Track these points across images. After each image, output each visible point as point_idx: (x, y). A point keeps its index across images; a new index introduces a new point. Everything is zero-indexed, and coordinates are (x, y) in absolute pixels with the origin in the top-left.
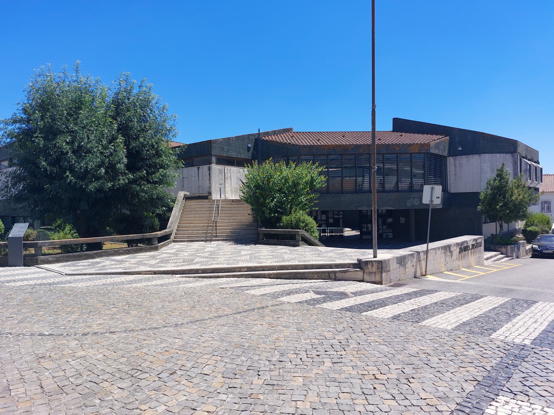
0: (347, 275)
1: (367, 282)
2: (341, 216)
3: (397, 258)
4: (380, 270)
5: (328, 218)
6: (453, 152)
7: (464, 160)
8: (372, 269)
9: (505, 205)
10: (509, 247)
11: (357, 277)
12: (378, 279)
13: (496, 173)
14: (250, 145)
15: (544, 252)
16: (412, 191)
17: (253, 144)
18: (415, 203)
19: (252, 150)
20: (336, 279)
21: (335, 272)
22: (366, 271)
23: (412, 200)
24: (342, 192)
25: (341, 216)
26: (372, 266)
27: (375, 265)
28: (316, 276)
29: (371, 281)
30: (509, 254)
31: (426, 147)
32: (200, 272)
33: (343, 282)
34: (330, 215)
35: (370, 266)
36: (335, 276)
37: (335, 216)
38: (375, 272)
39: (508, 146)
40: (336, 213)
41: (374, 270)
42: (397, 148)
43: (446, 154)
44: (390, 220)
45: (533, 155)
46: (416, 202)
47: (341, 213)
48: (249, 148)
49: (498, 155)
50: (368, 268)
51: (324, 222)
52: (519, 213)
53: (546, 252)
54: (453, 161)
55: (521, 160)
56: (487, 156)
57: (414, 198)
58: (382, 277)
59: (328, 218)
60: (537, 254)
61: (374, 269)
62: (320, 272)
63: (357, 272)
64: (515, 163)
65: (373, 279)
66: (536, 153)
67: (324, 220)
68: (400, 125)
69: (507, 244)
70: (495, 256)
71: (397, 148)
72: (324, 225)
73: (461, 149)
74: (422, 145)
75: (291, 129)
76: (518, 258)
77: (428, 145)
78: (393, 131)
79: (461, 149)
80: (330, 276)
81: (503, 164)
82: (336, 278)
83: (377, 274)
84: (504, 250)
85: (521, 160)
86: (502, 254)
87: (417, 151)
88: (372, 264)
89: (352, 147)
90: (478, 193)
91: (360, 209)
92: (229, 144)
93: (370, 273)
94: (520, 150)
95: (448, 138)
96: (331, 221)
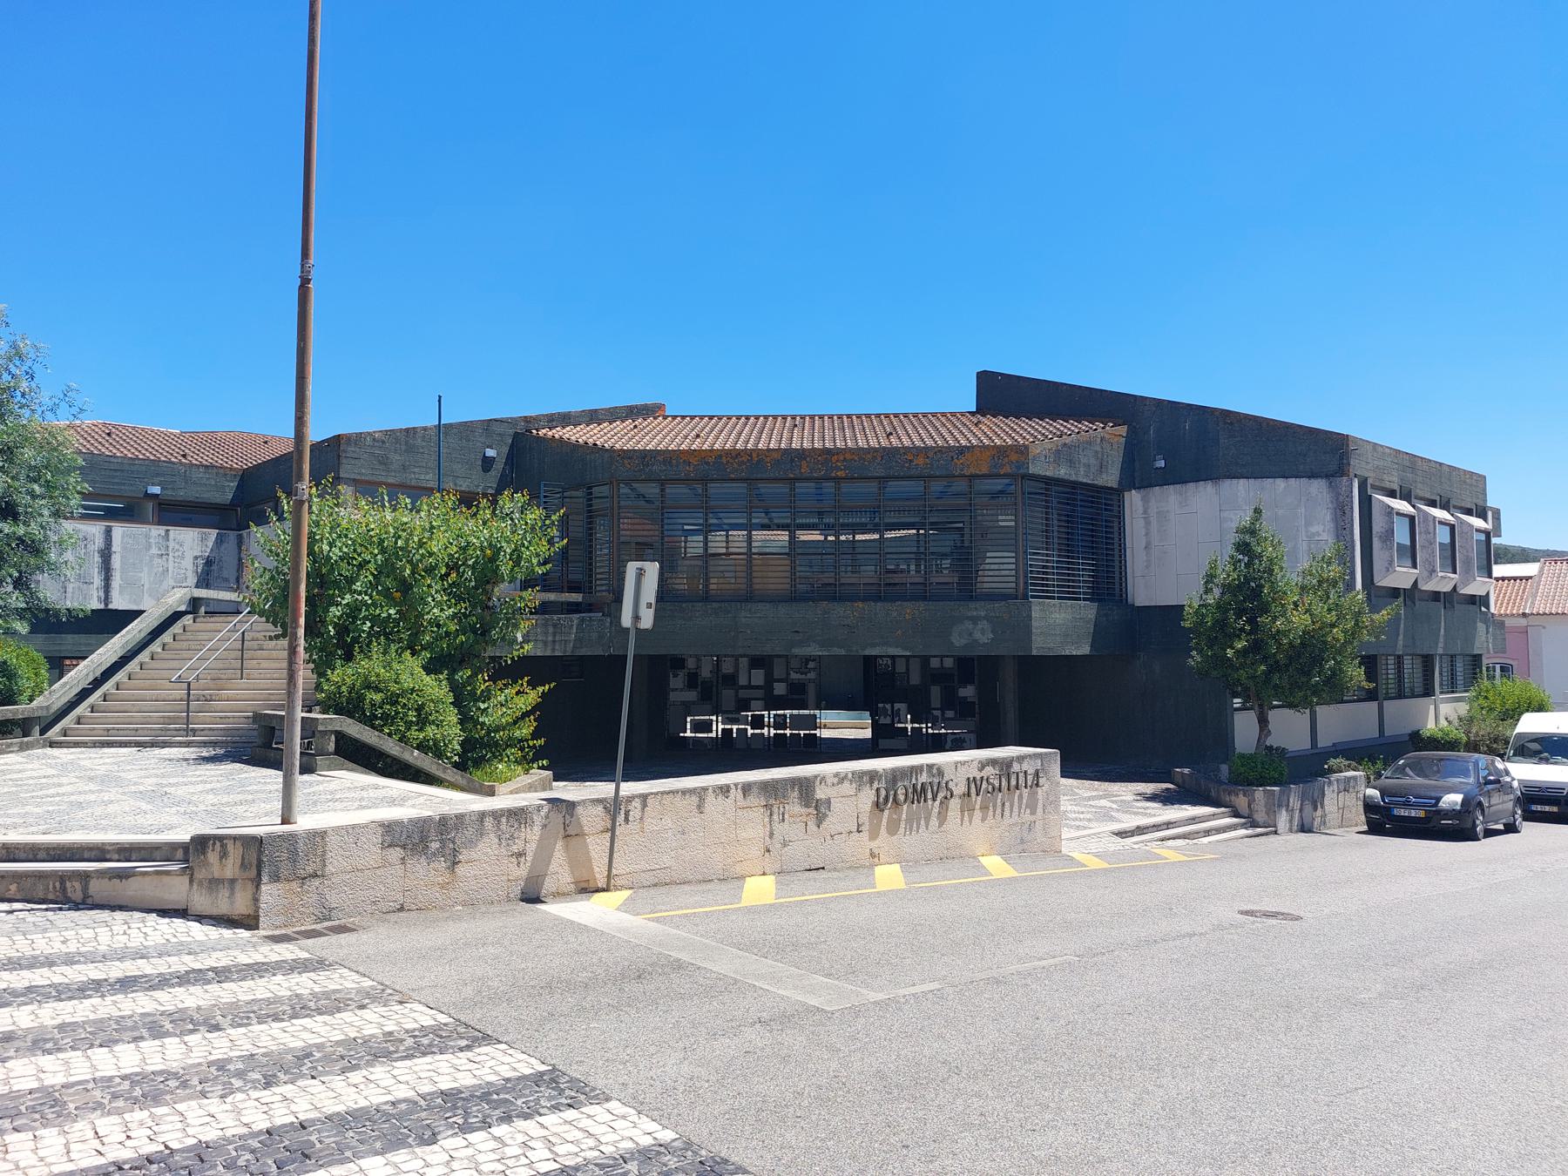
0: (132, 889)
1: (200, 918)
2: (812, 675)
3: (382, 824)
4: (254, 872)
5: (770, 680)
6: (1138, 474)
7: (1170, 499)
8: (223, 866)
9: (1256, 647)
10: (1259, 793)
11: (167, 896)
12: (241, 906)
13: (1233, 538)
14: (490, 453)
15: (1396, 812)
16: (971, 598)
17: (506, 450)
18: (977, 635)
19: (499, 466)
20: (85, 903)
21: (85, 876)
22: (199, 875)
23: (968, 625)
24: (749, 597)
25: (812, 675)
26: (224, 855)
27: (235, 852)
28: (13, 887)
29: (215, 912)
30: (1260, 817)
31: (1014, 457)
32: (41, 855)
33: (105, 915)
34: (778, 672)
35: (212, 857)
36: (85, 889)
37: (794, 676)
38: (233, 881)
39: (1317, 455)
40: (794, 664)
41: (229, 874)
42: (920, 461)
43: (1110, 479)
44: (968, 692)
45: (1462, 492)
46: (983, 631)
47: (811, 665)
48: (487, 463)
49: (1281, 483)
50: (206, 864)
51: (760, 693)
52: (1309, 674)
53: (1403, 812)
54: (1140, 503)
55: (1366, 502)
56: (1241, 485)
57: (975, 620)
58: (256, 900)
59: (770, 680)
60: (1382, 821)
61: (230, 869)
62: (54, 873)
63: (166, 879)
64: (1342, 511)
65: (223, 907)
66: (1477, 482)
67: (757, 687)
68: (1000, 395)
69: (1262, 782)
70: (1213, 817)
71: (920, 461)
72: (760, 703)
73: (1162, 463)
74: (1002, 451)
75: (661, 407)
76: (1305, 828)
77: (1022, 450)
78: (982, 409)
79: (1162, 463)
80: (64, 889)
81: (1257, 511)
82: (86, 896)
83: (238, 886)
84: (1241, 801)
85: (1366, 502)
86: (1236, 815)
87: (985, 471)
88: (223, 846)
89: (775, 455)
90: (1180, 608)
91: (867, 653)
92: (411, 449)
93: (214, 883)
94: (1358, 466)
95: (1123, 430)
96: (780, 689)
